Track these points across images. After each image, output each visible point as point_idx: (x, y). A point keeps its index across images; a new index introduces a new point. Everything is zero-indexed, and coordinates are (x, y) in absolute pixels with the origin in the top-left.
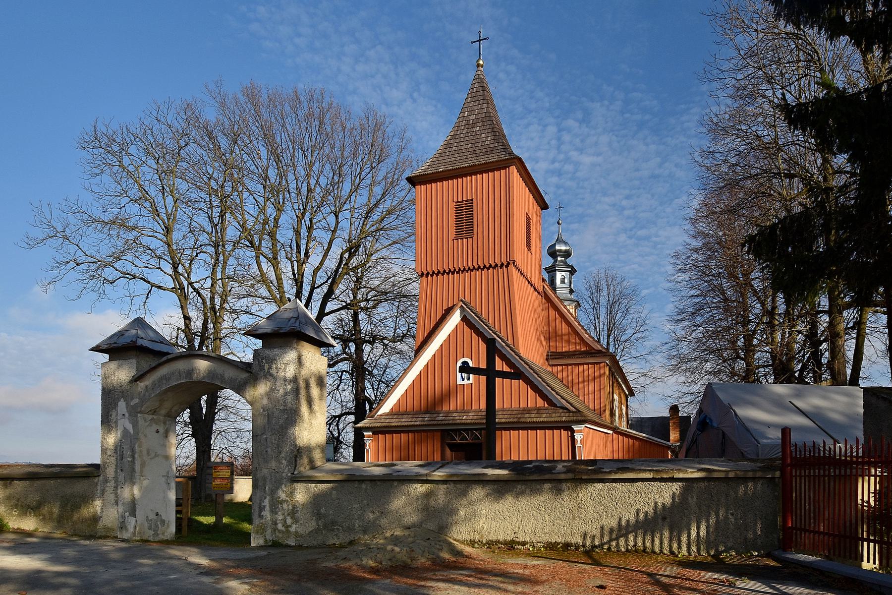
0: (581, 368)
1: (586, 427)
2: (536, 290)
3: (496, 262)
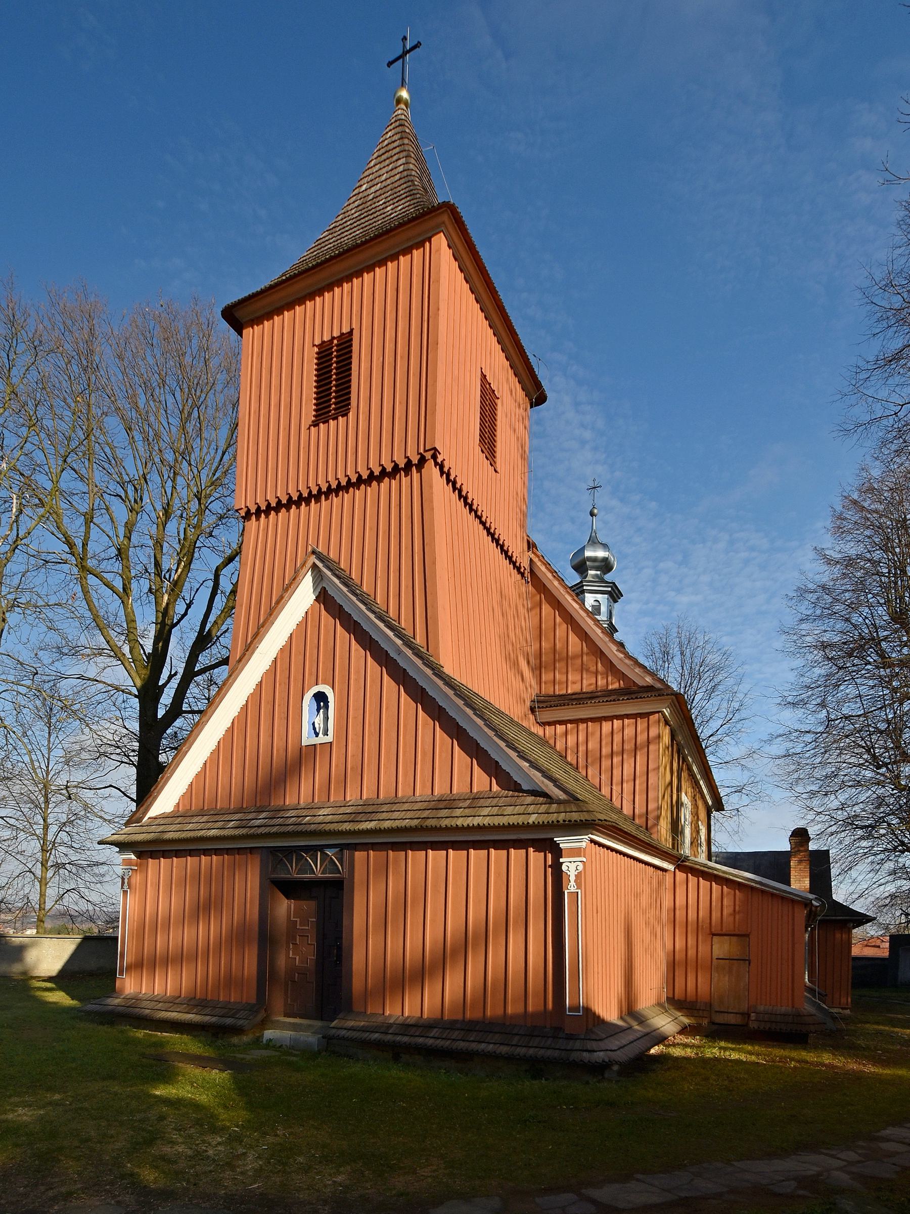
0: (606, 726)
1: (592, 841)
2: (509, 558)
3: (395, 459)
